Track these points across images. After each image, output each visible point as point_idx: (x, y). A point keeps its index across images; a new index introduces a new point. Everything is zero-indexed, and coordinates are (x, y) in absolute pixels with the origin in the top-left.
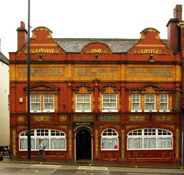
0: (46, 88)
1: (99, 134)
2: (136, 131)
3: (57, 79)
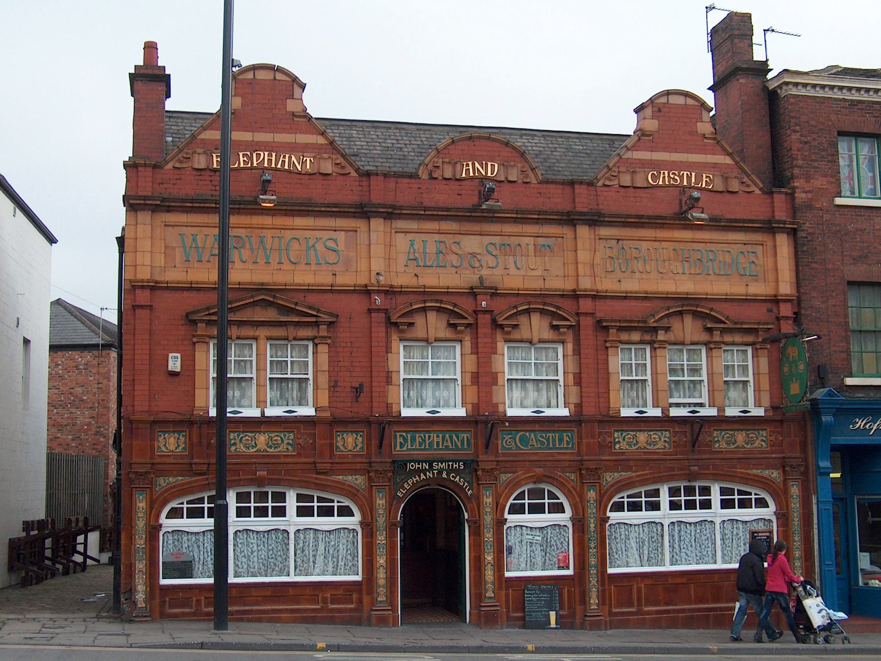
1: (498, 507)
2: (639, 495)
3: (324, 279)
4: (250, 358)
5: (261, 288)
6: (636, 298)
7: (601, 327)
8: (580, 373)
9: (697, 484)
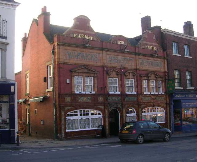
0: (87, 70)
2: (73, 112)
3: (95, 64)
4: (77, 80)
5: (84, 65)
6: (145, 71)
7: (140, 76)
8: (122, 85)
9: (86, 110)
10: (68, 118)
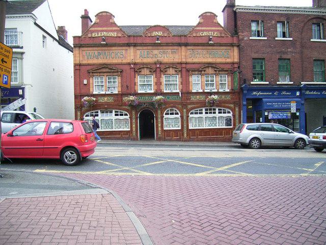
2: (93, 113)
9: (212, 108)
10: (191, 116)
